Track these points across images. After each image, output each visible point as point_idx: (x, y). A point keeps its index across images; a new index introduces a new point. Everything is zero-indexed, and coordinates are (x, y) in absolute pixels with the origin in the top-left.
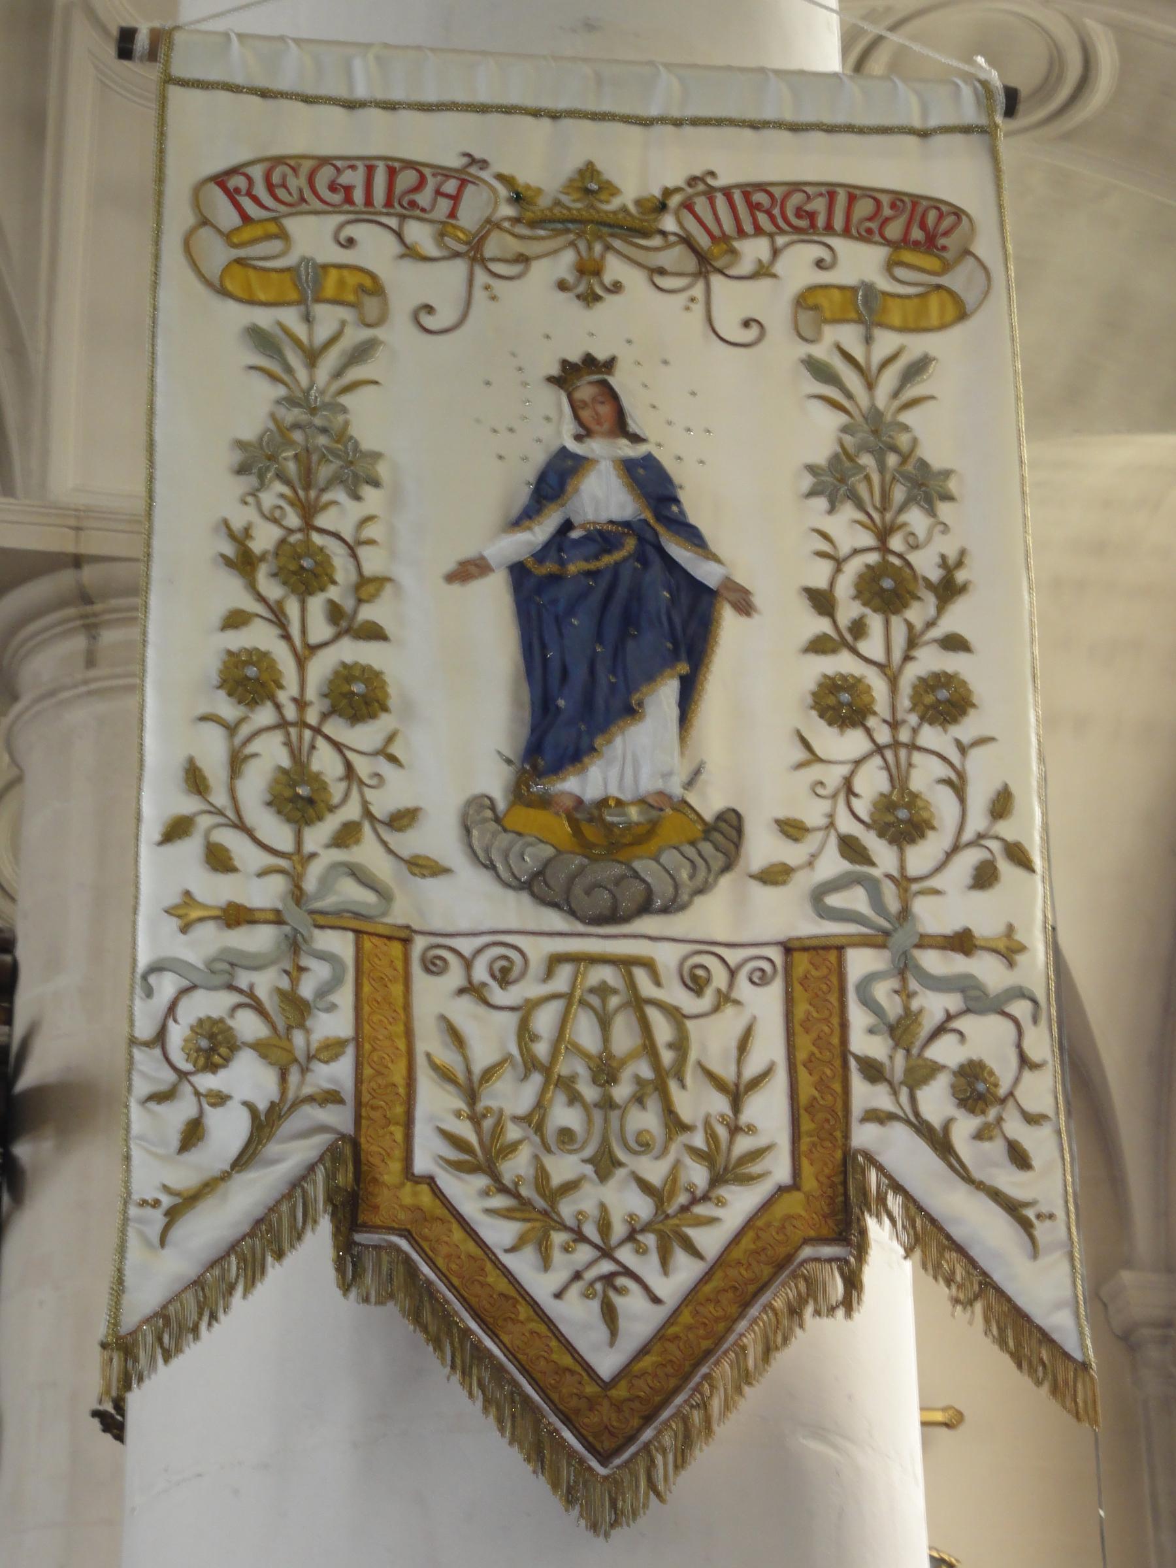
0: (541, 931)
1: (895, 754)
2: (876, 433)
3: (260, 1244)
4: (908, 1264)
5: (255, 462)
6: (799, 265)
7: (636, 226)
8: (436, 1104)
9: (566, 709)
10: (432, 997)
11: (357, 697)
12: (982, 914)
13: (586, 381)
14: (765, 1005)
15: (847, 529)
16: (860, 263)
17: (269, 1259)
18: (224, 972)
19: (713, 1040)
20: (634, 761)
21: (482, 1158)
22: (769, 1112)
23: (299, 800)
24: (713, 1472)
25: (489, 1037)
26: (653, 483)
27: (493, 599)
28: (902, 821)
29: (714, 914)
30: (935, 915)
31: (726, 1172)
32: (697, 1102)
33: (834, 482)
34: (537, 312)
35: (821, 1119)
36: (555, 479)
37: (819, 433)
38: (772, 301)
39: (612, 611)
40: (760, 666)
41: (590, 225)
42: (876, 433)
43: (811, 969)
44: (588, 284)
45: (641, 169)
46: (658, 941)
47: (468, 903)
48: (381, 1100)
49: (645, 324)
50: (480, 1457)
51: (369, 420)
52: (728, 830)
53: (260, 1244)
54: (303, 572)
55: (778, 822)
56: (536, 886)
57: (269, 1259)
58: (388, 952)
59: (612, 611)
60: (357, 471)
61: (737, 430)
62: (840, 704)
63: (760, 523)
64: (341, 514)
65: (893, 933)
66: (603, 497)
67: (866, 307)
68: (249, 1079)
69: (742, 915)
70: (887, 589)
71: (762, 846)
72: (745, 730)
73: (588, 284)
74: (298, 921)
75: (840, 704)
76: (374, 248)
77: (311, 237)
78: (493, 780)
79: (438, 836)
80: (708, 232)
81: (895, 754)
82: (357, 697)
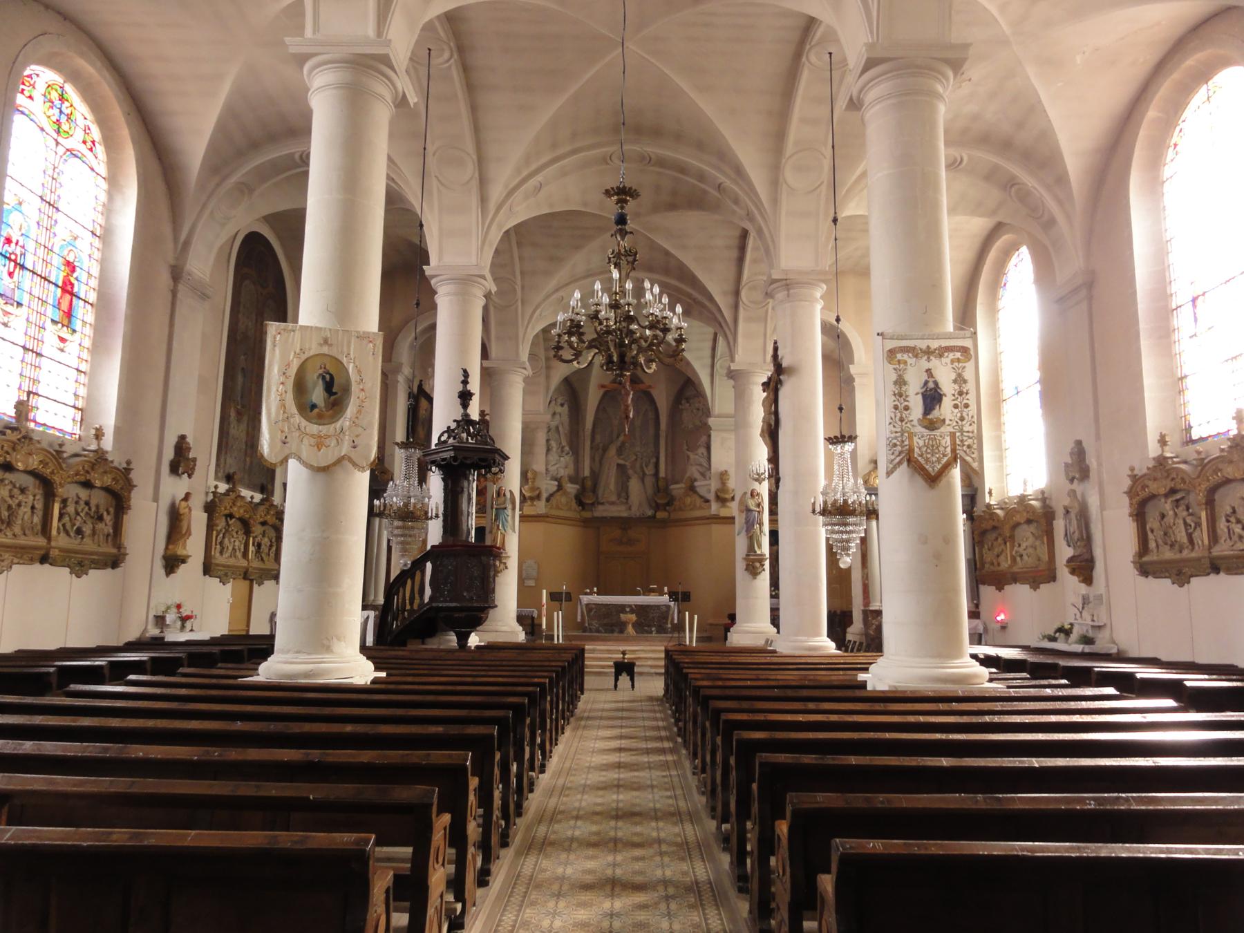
0: (926, 432)
1: (961, 412)
2: (959, 375)
3: (900, 463)
4: (1186, 371)
5: (895, 383)
6: (951, 356)
7: (933, 352)
8: (916, 450)
9: (928, 409)
10: (915, 439)
11: (907, 408)
12: (970, 429)
13: (929, 371)
14: (948, 439)
15: (957, 387)
16: (958, 355)
17: (267, 671)
18: (896, 438)
19: (943, 442)
20: (935, 414)
21: (921, 455)
22: (949, 450)
23: (902, 420)
24: (944, 480)
25: (921, 443)
26: (936, 383)
27: (920, 396)
28: (962, 419)
29: (942, 429)
30: (965, 429)
31: (944, 455)
32: (941, 449)
33: (955, 381)
34: (924, 364)
35: (954, 451)
36: (926, 383)
37: (953, 376)
38: (948, 361)
39: (932, 397)
40: (947, 403)
41: (928, 352)
42: (959, 375)
43: (953, 435)
44: (929, 360)
45: (935, 344)
46: (937, 433)
47: (919, 429)
48: (911, 450)
49: (935, 363)
50: (920, 481)
51: (907, 377)
52: (944, 421)
53: (900, 463)
54: (901, 395)
55: (168, 574)
56: (926, 427)
57: (267, 671)
58: (911, 436)
59: (932, 397)
60: (905, 383)
61: (945, 378)
62: (956, 406)
63: (948, 387)
64: (904, 388)
65: (962, 431)
66: (931, 385)
67: (959, 360)
68: (899, 448)
69: (945, 429)
70: (961, 393)
71: (947, 422)
72: (946, 409)
73: (929, 360)
74: (902, 432)
75: (956, 406)
76: (905, 357)
77: (899, 356)
78: (920, 416)
79: (915, 422)
80: (941, 352)
81: (961, 412)
82: (907, 408)
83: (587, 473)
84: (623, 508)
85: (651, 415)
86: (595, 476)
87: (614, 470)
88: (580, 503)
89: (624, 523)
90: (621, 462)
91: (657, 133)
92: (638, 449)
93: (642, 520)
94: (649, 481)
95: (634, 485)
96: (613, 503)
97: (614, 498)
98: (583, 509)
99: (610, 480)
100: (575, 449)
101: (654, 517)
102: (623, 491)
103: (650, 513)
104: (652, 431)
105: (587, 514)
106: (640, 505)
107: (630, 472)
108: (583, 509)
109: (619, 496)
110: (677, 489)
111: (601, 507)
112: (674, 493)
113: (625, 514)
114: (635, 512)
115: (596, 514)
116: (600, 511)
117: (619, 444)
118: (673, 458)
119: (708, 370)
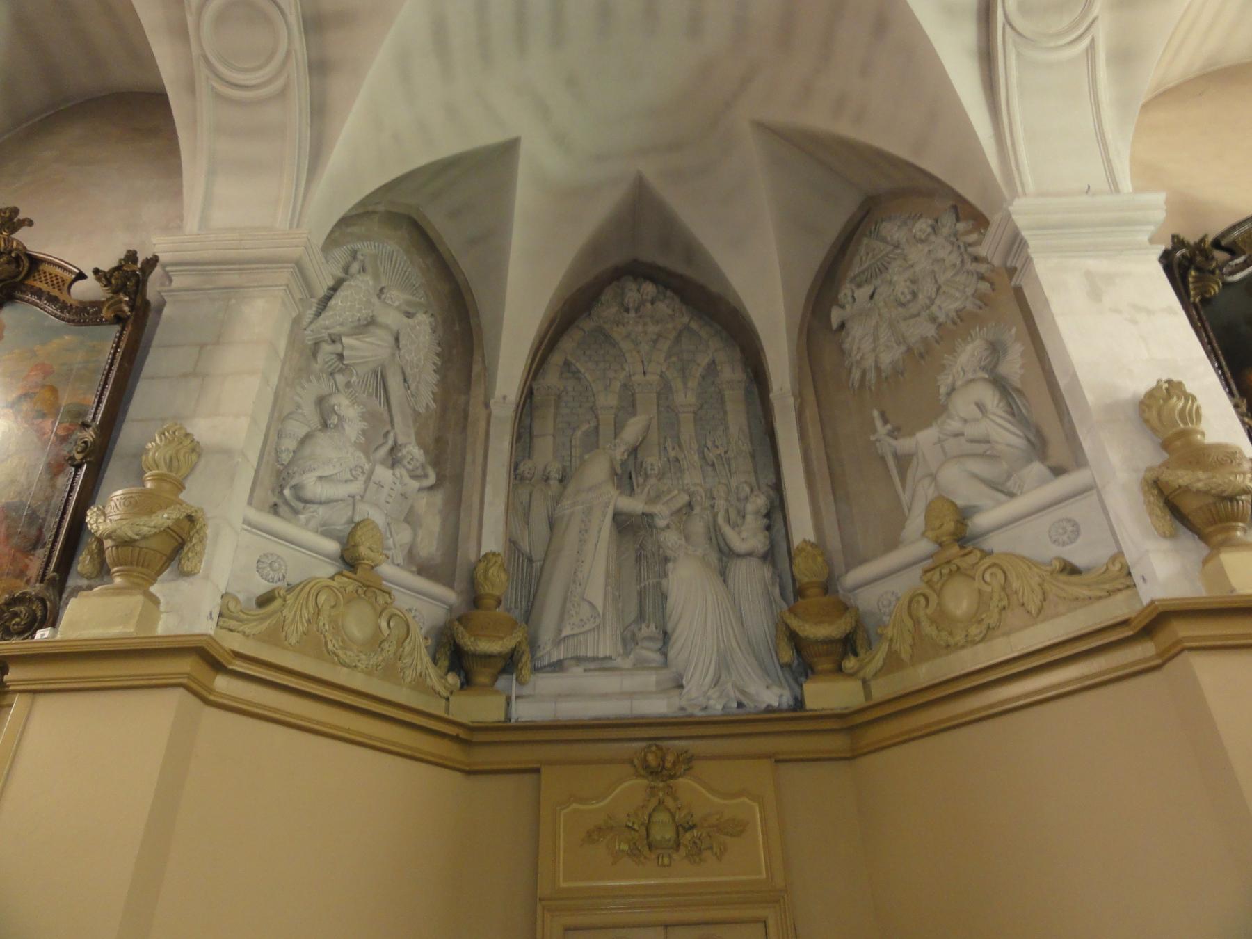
83: (492, 542)
84: (649, 680)
85: (732, 374)
86: (530, 571)
87: (604, 529)
88: (457, 658)
89: (660, 749)
90: (634, 505)
91: (470, 736)
92: (692, 479)
93: (742, 724)
94: (751, 579)
95: (689, 584)
96: (602, 664)
97: (605, 645)
98: (467, 683)
99: (589, 570)
100: (448, 460)
101: (799, 703)
102: (647, 619)
103: (773, 696)
104: (737, 419)
105: (480, 708)
106: (724, 664)
107: (671, 539)
108: (467, 683)
109: (629, 641)
110: (882, 582)
111: (546, 683)
112: (867, 600)
113: (658, 706)
114: (703, 694)
115: (524, 712)
116: (539, 700)
117: (620, 453)
118: (832, 477)
119: (968, 34)
